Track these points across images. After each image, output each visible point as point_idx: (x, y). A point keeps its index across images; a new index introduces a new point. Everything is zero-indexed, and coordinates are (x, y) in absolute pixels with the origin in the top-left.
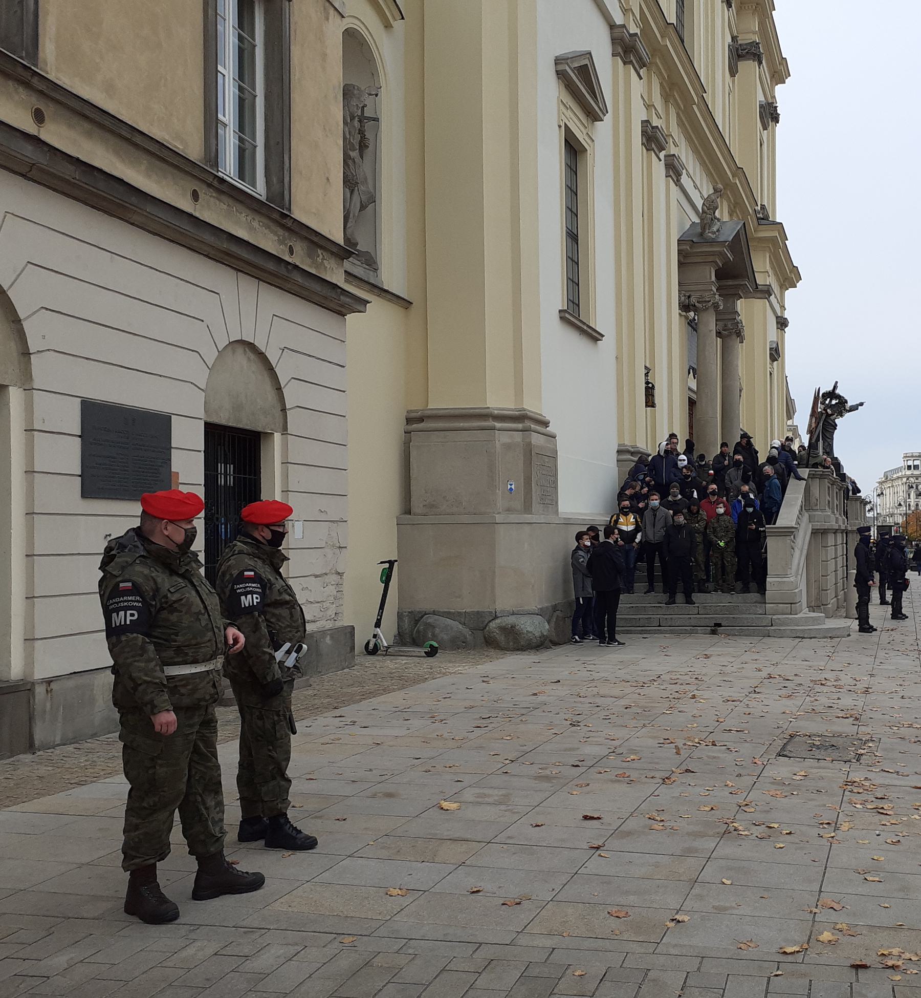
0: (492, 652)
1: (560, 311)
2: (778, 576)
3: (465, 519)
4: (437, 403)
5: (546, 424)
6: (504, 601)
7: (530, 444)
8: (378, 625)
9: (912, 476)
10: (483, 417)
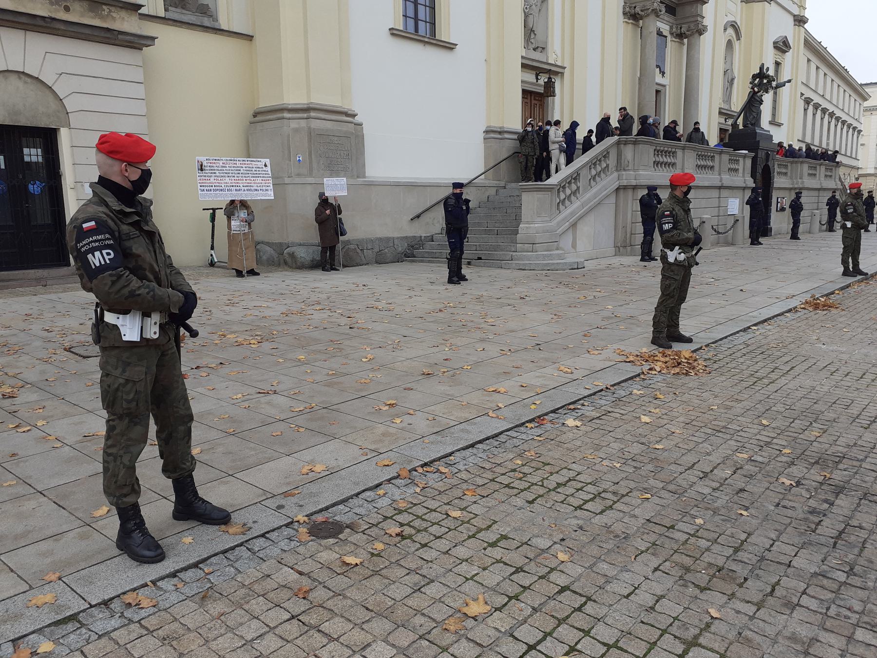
1: (390, 29)
2: (528, 223)
4: (265, 103)
7: (309, 128)
8: (212, 248)
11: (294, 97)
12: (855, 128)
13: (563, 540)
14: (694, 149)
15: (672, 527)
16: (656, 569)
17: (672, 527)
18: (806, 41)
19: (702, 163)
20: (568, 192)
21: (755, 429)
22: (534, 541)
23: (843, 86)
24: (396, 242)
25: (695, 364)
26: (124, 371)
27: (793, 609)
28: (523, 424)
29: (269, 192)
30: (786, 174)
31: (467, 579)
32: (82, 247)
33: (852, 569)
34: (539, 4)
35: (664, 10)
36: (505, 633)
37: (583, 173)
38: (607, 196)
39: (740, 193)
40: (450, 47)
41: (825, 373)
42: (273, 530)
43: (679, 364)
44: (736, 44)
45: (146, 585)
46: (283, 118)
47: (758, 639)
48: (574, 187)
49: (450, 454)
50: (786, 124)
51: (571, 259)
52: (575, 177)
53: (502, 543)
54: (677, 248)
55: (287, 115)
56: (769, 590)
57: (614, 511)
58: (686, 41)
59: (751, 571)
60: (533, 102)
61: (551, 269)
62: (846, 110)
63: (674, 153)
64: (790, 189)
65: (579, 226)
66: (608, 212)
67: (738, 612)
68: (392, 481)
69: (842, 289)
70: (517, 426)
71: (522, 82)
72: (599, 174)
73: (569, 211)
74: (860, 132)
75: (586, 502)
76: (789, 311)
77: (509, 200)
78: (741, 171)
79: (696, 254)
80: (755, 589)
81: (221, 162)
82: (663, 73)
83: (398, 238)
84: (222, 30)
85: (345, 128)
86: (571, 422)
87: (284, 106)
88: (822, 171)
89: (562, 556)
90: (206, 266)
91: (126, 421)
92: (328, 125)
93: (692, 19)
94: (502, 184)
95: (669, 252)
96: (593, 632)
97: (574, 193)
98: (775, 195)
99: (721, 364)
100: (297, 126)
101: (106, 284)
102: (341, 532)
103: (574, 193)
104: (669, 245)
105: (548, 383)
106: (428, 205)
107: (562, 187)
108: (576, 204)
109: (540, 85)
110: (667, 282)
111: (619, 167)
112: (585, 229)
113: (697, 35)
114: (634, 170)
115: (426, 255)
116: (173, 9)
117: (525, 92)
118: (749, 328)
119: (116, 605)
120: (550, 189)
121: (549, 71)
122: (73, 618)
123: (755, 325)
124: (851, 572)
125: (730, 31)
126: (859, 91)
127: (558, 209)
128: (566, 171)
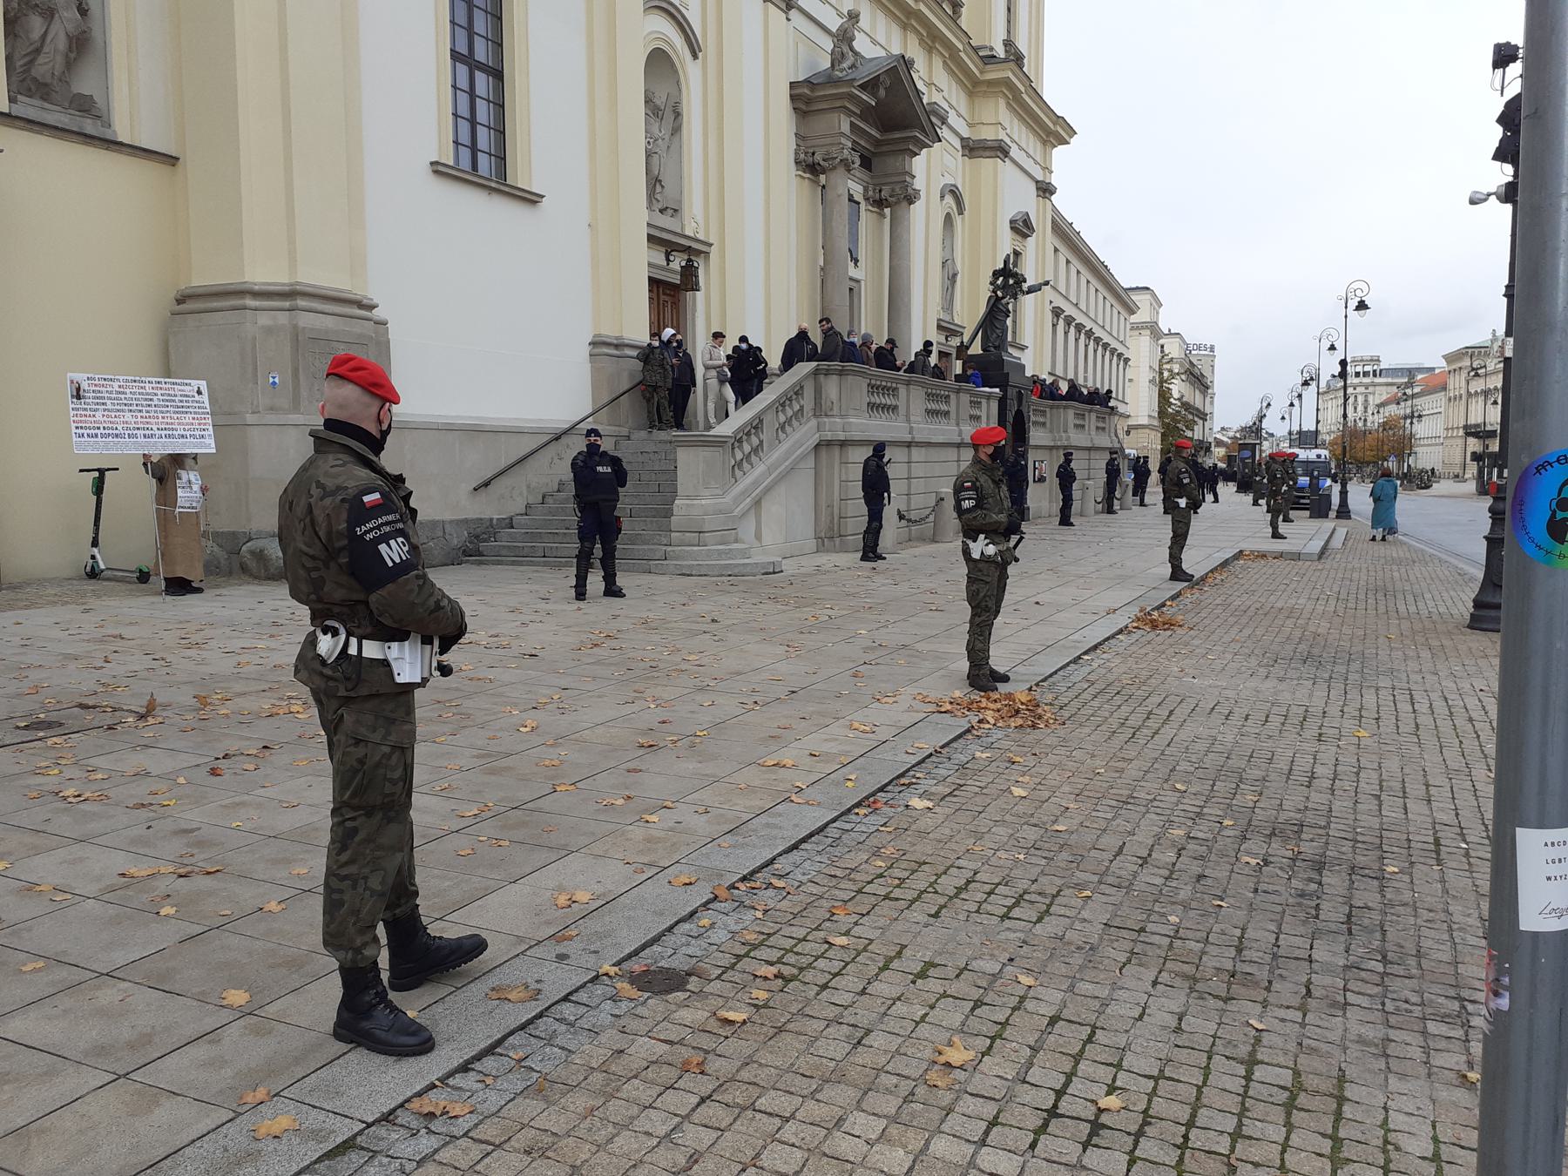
2: (688, 497)
4: (202, 279)
7: (295, 327)
8: (95, 543)
9: (1361, 384)
11: (263, 272)
12: (1120, 355)
13: (1011, 960)
14: (922, 385)
15: (1142, 930)
16: (1155, 983)
17: (1142, 930)
18: (1054, 222)
19: (934, 406)
20: (747, 448)
21: (1172, 797)
22: (974, 965)
23: (1103, 291)
24: (447, 527)
25: (1040, 711)
26: (388, 733)
27: (1344, 1010)
28: (849, 810)
29: (207, 441)
30: (1044, 424)
31: (917, 1023)
32: (366, 532)
33: (1384, 957)
35: (858, 162)
36: (1013, 1080)
37: (767, 419)
38: (803, 457)
40: (530, 199)
41: (1217, 719)
42: (576, 991)
43: (1017, 712)
44: (958, 220)
45: (433, 1086)
46: (245, 308)
47: (1324, 1047)
49: (771, 861)
50: (1037, 350)
51: (758, 558)
52: (756, 425)
54: (982, 536)
56: (1304, 991)
58: (887, 211)
59: (1271, 972)
60: (662, 297)
61: (734, 574)
62: (1108, 327)
63: (895, 389)
64: (1051, 448)
66: (803, 486)
67: (1283, 1020)
69: (1173, 598)
70: (842, 814)
71: (650, 264)
72: (789, 421)
73: (749, 480)
74: (1127, 360)
75: (1010, 908)
76: (1120, 632)
77: (641, 458)
79: (1015, 547)
80: (1287, 991)
81: (116, 385)
83: (451, 522)
84: (121, 144)
85: (358, 328)
86: (917, 803)
87: (247, 286)
88: (1092, 420)
89: (1026, 980)
90: (80, 579)
91: (380, 815)
92: (328, 323)
94: (625, 431)
95: (971, 545)
96: (1125, 1064)
99: (1072, 709)
101: (411, 591)
103: (755, 450)
104: (970, 533)
105: (848, 748)
106: (503, 464)
107: (738, 440)
108: (760, 469)
109: (673, 271)
110: (974, 587)
112: (774, 509)
113: (905, 204)
114: (842, 416)
115: (504, 552)
116: (27, 100)
117: (653, 281)
118: (1079, 657)
119: (403, 1117)
120: (719, 442)
121: (688, 249)
122: (348, 1145)
123: (1086, 653)
124: (1384, 960)
125: (949, 199)
126: (1123, 298)
127: (733, 475)
128: (740, 417)
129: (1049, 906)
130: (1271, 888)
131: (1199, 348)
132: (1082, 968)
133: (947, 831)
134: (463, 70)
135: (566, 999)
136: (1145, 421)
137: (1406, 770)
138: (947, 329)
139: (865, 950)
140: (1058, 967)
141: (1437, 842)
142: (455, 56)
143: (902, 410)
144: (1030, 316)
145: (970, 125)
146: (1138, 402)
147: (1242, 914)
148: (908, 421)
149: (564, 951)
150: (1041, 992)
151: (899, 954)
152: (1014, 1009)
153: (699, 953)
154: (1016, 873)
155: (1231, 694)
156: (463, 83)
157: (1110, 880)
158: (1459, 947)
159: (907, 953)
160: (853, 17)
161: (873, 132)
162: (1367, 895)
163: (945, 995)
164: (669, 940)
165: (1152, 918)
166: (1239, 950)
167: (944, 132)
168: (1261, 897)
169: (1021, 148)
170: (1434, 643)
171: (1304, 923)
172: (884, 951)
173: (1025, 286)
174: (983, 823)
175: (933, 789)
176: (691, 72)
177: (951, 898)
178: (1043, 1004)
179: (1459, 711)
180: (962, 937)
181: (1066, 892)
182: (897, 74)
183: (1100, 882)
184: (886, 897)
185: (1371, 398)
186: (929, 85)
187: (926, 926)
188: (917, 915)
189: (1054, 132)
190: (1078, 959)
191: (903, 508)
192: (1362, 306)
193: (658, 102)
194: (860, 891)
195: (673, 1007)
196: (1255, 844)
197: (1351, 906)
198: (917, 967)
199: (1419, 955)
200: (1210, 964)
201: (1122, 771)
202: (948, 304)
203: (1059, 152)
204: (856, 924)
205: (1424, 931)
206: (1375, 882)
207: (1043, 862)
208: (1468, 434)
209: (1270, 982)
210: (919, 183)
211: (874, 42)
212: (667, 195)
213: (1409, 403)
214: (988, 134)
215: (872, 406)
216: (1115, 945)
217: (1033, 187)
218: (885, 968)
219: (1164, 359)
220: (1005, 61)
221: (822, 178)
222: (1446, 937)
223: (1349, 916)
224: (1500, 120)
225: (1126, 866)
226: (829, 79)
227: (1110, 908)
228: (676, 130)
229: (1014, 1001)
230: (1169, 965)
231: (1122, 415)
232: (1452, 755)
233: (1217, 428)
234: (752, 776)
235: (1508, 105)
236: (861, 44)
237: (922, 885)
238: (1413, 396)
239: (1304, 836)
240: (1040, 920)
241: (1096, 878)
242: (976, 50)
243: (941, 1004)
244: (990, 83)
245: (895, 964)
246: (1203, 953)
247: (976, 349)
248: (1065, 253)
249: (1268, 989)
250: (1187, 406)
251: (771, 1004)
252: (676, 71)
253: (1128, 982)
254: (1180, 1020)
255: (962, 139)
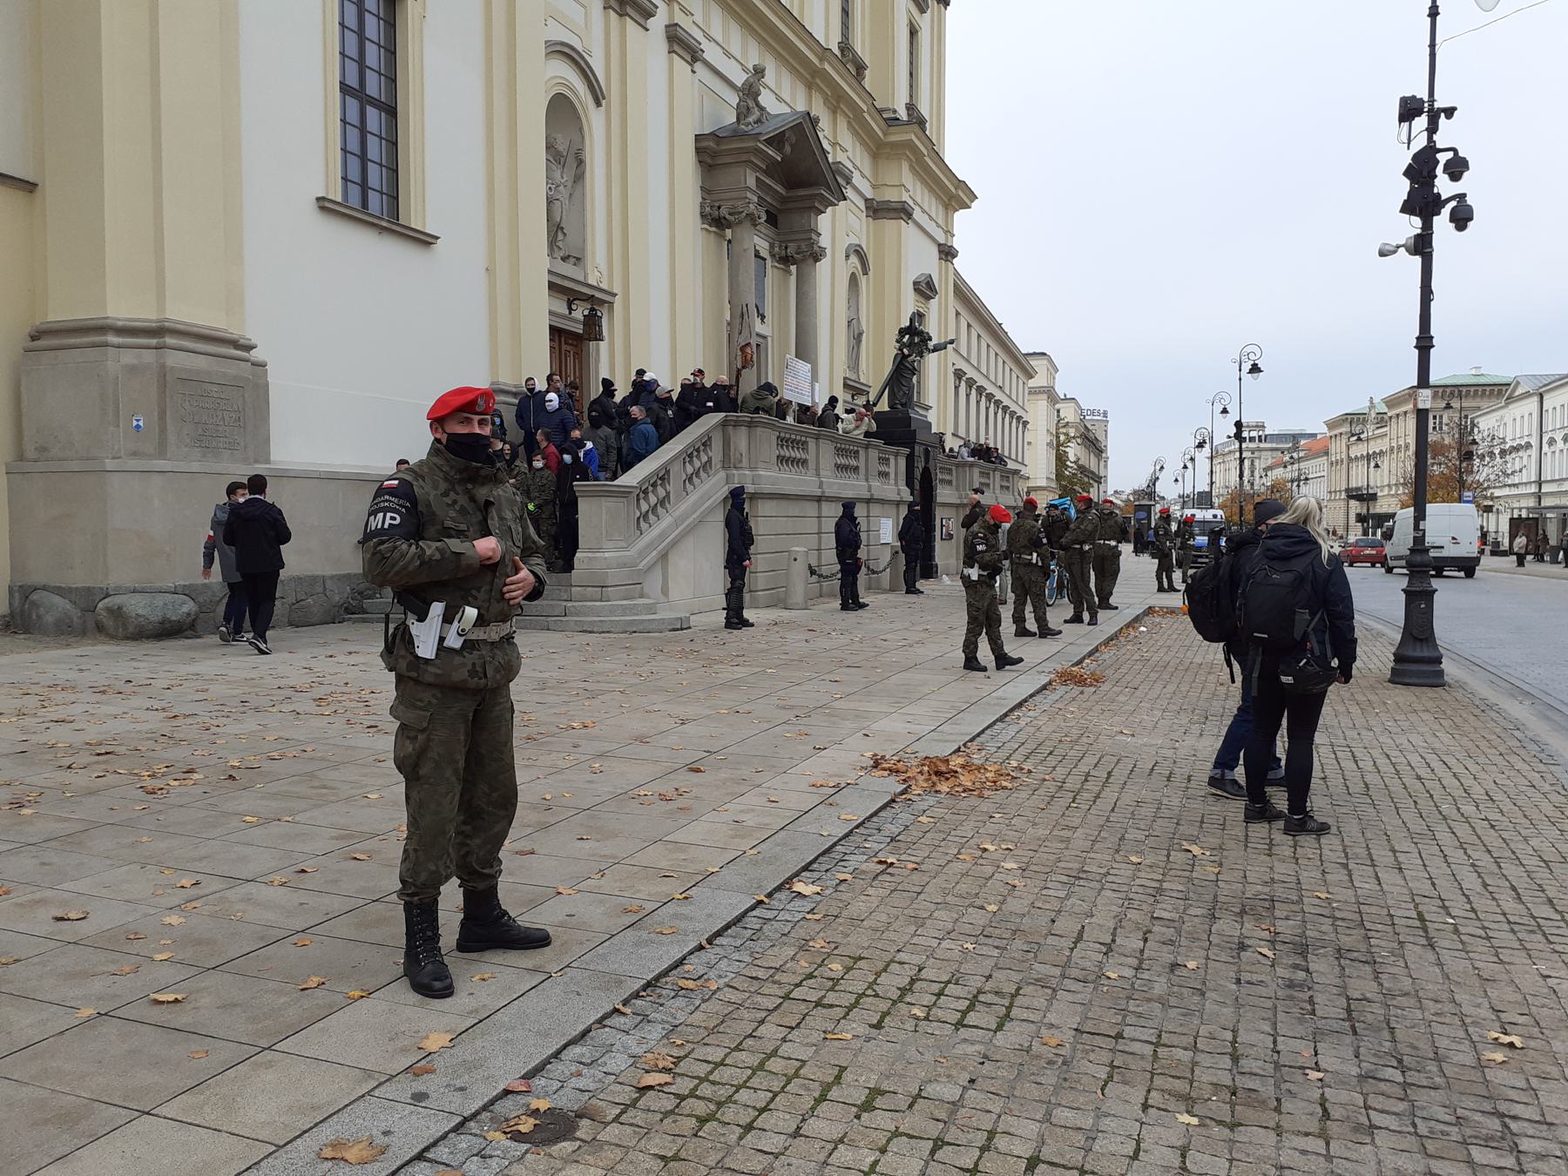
0: (102, 638)
1: (318, 199)
2: (590, 550)
3: (75, 466)
4: (58, 313)
5: (249, 348)
6: (119, 574)
7: (163, 366)
10: (94, 331)
11: (123, 306)
12: (1019, 418)
13: (972, 1081)
16: (1145, 1107)
17: (1119, 1036)
18: (955, 285)
19: (843, 461)
20: (653, 499)
21: (1126, 871)
22: (930, 1090)
23: (1003, 355)
24: (329, 584)
30: (950, 482)
33: (1400, 1061)
34: (569, 184)
35: (764, 217)
37: (675, 469)
38: (711, 510)
39: (892, 510)
40: (425, 240)
42: (434, 1144)
44: (863, 280)
48: (661, 492)
49: (680, 962)
50: (941, 409)
51: (664, 614)
53: (879, 1102)
55: (112, 339)
56: (1319, 1110)
57: (1015, 1023)
58: (793, 268)
59: (1277, 1086)
60: (564, 347)
61: (632, 630)
64: (957, 506)
65: (672, 558)
67: (1304, 1152)
68: (607, 1022)
71: (551, 313)
74: (1025, 423)
75: (964, 1013)
78: (892, 476)
80: (1300, 1112)
82: (763, 317)
83: (332, 577)
85: (233, 369)
92: (201, 363)
93: (803, 236)
97: (662, 502)
98: (939, 513)
100: (135, 361)
102: (575, 1128)
108: (666, 521)
109: (576, 321)
111: (727, 463)
113: (811, 261)
120: (624, 493)
124: (1401, 1066)
125: (854, 259)
126: (1022, 363)
129: (1009, 1008)
130: (1255, 978)
131: (1093, 413)
132: (1057, 1089)
133: (884, 918)
134: (353, 104)
135: (420, 1157)
136: (1043, 483)
137: (1369, 835)
138: (853, 388)
139: (796, 1075)
140: (1028, 1089)
141: (1421, 917)
142: (345, 89)
143: (812, 464)
144: (934, 373)
145: (874, 187)
146: (1038, 469)
147: (1228, 1011)
148: (818, 475)
149: (422, 1088)
150: (1008, 1122)
151: (838, 1078)
152: (984, 1149)
153: (592, 1087)
154: (965, 968)
155: (1170, 753)
156: (353, 116)
157: (1074, 973)
158: (1479, 1046)
159: (848, 1077)
160: (759, 72)
161: (779, 188)
162: (1362, 985)
163: (897, 1134)
164: (557, 1068)
165: (1129, 1020)
166: (1235, 1059)
167: (849, 192)
168: (1245, 989)
169: (924, 211)
170: (1360, 697)
171: (1301, 1021)
172: (819, 1075)
173: (931, 344)
174: (923, 906)
175: (864, 867)
176: (595, 120)
177: (894, 1002)
178: (1017, 1141)
179: (1404, 768)
180: (912, 1053)
181: (1026, 990)
182: (801, 132)
183: (1063, 976)
184: (818, 1004)
185: (1257, 463)
186: (834, 144)
187: (868, 1040)
188: (855, 1027)
189: (956, 196)
190: (1050, 1078)
191: (814, 563)
192: (1255, 369)
193: (561, 148)
194: (786, 997)
195: (558, 1164)
196: (1227, 926)
197: (1348, 998)
198: (860, 1097)
199: (1438, 1059)
200: (1205, 1079)
201: (1068, 840)
202: (854, 363)
203: (960, 217)
204: (784, 1040)
205: (1437, 1028)
206: (1368, 968)
207: (996, 953)
208: (1350, 497)
209: (1278, 1100)
210: (824, 241)
211: (779, 99)
212: (568, 244)
213: (1296, 466)
214: (891, 195)
215: (782, 459)
216: (1092, 1056)
217: (935, 251)
218: (822, 1098)
219: (1060, 423)
220: (908, 123)
221: (728, 232)
222: (1462, 1034)
223: (1349, 1011)
224: (1406, 174)
225: (1088, 955)
226: (735, 134)
227: (1079, 1008)
228: (579, 178)
229: (981, 1138)
230: (1158, 1081)
231: (1022, 477)
232: (1409, 816)
233: (1110, 492)
234: (658, 857)
235: (1415, 157)
236: (766, 99)
237: (860, 987)
238: (1299, 460)
239: (1277, 913)
240: (1000, 1027)
241: (1058, 971)
242: (880, 111)
243: (893, 1147)
244: (894, 145)
245: (834, 1093)
246: (1195, 1064)
247: (883, 406)
248: (966, 317)
249: (1278, 1110)
250: (1082, 469)
251: (683, 1154)
252: (579, 118)
253: (1111, 1105)
254: (1183, 1156)
255: (866, 200)
